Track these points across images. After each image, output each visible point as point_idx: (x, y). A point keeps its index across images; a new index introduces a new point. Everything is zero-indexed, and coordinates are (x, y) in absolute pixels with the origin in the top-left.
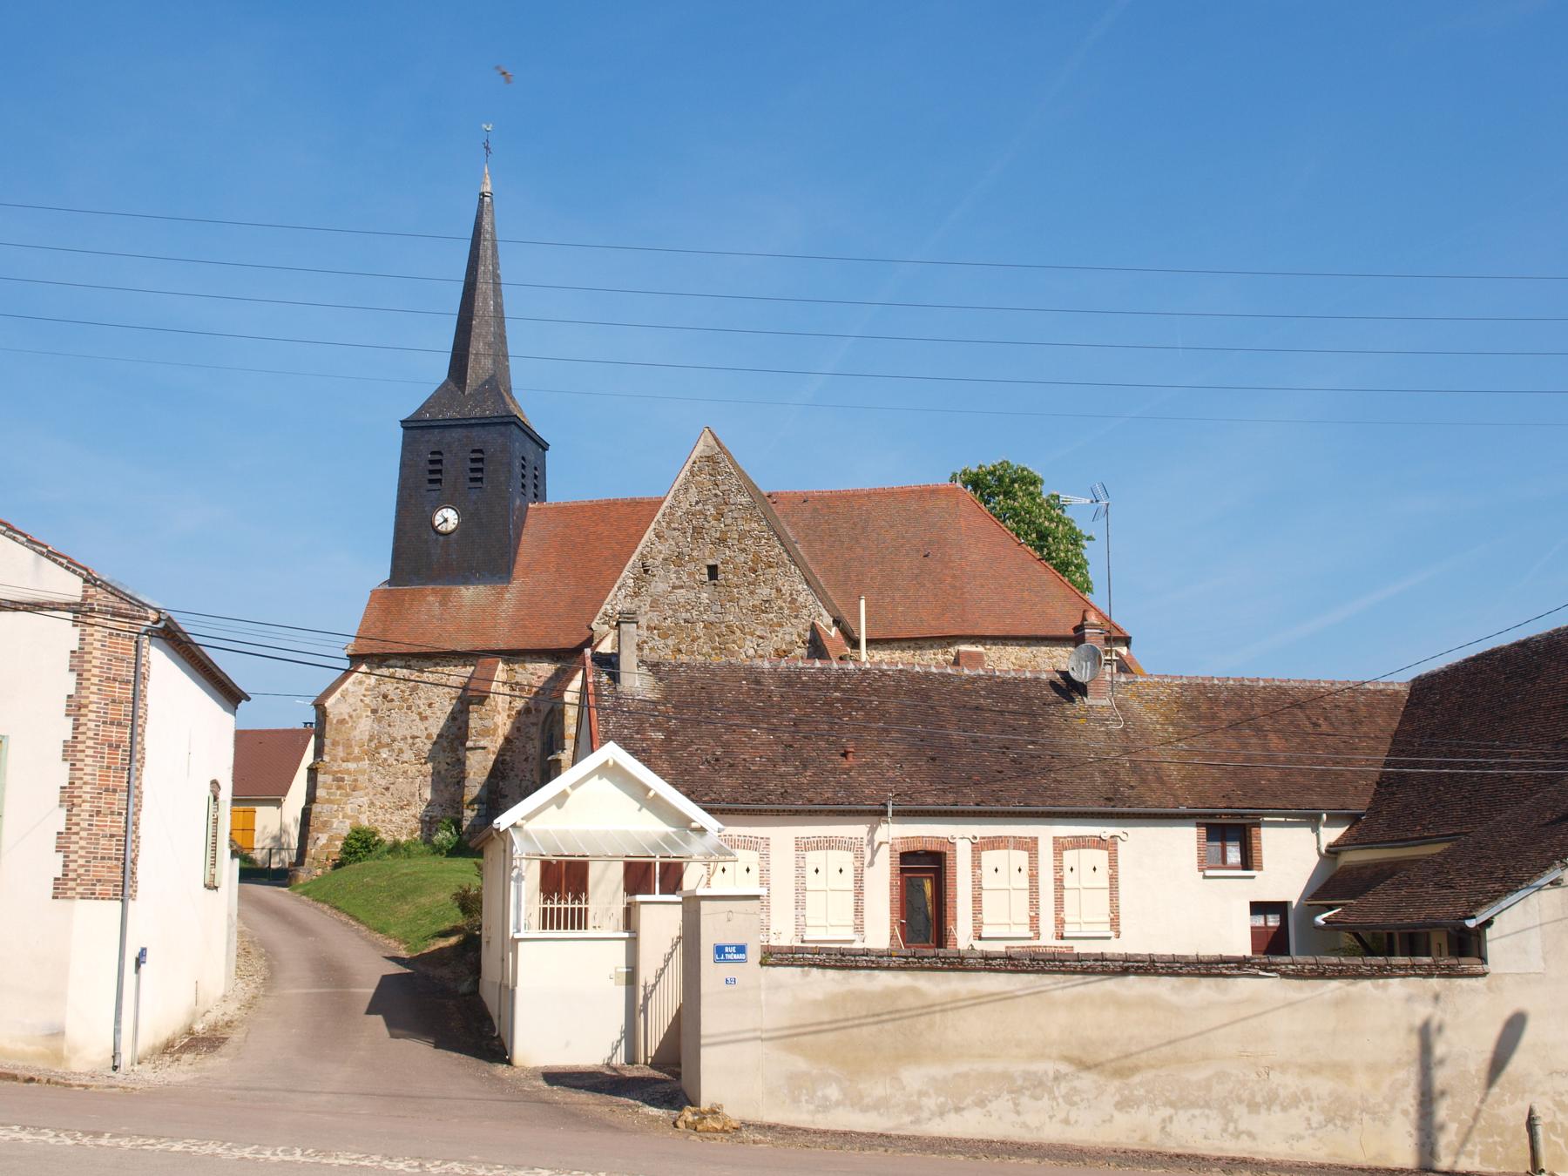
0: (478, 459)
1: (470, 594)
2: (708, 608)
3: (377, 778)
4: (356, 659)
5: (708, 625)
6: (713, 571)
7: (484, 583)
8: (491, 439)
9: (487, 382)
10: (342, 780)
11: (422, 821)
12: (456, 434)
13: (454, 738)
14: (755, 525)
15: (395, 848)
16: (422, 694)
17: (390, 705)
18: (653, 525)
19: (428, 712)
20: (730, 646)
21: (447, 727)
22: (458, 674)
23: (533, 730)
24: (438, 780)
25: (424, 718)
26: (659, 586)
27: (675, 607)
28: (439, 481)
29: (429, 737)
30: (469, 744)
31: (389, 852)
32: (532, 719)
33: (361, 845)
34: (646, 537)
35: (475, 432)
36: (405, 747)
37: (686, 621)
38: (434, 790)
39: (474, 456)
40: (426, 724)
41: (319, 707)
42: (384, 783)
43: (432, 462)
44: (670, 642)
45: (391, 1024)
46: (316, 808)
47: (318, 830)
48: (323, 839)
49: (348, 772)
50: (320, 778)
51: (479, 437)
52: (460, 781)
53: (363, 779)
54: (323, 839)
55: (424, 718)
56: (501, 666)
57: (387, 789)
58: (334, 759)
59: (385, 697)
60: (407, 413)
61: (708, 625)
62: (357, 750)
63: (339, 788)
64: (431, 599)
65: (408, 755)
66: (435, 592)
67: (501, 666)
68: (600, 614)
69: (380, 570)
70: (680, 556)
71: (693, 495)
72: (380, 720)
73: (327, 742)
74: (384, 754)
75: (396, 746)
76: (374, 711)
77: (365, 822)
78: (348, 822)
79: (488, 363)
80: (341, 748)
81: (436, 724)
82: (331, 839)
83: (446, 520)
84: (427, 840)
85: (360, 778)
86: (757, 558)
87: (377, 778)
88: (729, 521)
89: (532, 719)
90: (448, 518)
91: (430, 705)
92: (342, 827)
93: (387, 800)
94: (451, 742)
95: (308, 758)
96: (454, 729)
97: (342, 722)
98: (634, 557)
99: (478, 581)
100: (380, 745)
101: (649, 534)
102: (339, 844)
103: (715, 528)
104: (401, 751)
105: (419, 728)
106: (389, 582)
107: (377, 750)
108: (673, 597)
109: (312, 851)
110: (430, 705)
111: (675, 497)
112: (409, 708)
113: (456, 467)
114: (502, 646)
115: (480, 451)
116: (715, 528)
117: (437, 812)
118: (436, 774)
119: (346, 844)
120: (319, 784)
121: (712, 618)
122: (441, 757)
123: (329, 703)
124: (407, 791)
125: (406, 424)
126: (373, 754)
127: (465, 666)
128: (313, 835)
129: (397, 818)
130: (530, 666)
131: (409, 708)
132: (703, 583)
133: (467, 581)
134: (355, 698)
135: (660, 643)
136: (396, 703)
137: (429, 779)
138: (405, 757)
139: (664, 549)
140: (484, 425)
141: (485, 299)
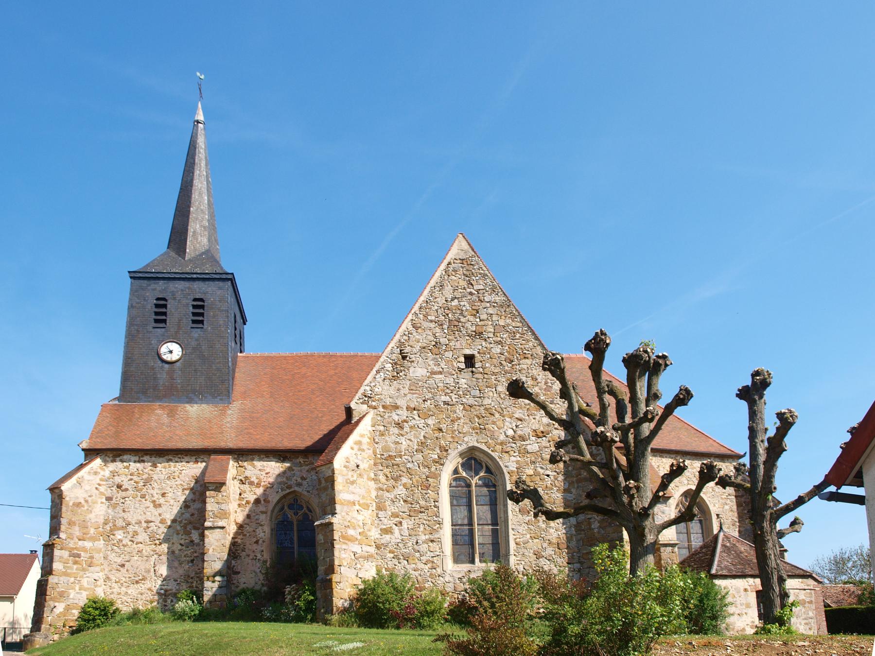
0: (199, 308)
1: (195, 410)
3: (112, 556)
4: (91, 453)
6: (470, 360)
7: (207, 403)
8: (213, 292)
9: (203, 253)
10: (79, 556)
11: (158, 593)
12: (181, 285)
13: (192, 520)
14: (509, 321)
15: (135, 615)
16: (155, 485)
17: (124, 494)
18: (410, 317)
19: (162, 501)
20: (490, 426)
21: (180, 513)
22: (191, 470)
23: (262, 517)
24: (173, 558)
25: (157, 506)
26: (418, 371)
27: (434, 390)
28: (164, 321)
29: (162, 521)
30: (207, 524)
31: (129, 619)
32: (262, 508)
33: (97, 614)
34: (403, 327)
35: (196, 285)
36: (140, 530)
37: (445, 403)
38: (170, 567)
39: (195, 303)
40: (160, 510)
41: (55, 491)
42: (119, 560)
43: (157, 306)
44: (430, 421)
46: (52, 580)
47: (54, 600)
48: (60, 608)
49: (85, 550)
50: (57, 553)
51: (199, 289)
52: (199, 557)
53: (98, 557)
54: (60, 608)
55: (157, 506)
56: (231, 462)
57: (123, 566)
58: (70, 537)
59: (119, 487)
60: (44, 542)
62: (92, 531)
63: (75, 563)
64: (159, 412)
65: (142, 537)
66: (163, 408)
67: (231, 462)
68: (359, 395)
69: (115, 390)
70: (437, 344)
71: (448, 292)
72: (115, 506)
73: (64, 521)
74: (119, 535)
75: (130, 529)
76: (109, 499)
77: (100, 593)
78: (84, 594)
79: (204, 241)
80: (77, 528)
81: (171, 510)
82: (68, 608)
83: (171, 352)
84: (164, 609)
85: (96, 556)
86: (513, 350)
87: (112, 556)
88: (484, 317)
89: (262, 508)
90: (172, 351)
91: (163, 495)
92: (79, 598)
93: (123, 575)
94: (185, 527)
95: (35, 573)
96: (187, 515)
97: (78, 505)
98: (392, 344)
99: (201, 401)
100: (115, 528)
101: (407, 325)
102: (76, 613)
103: (470, 324)
104: (136, 533)
105: (153, 514)
106: (118, 399)
107: (112, 532)
108: (431, 381)
109: (48, 617)
110: (163, 495)
111: (431, 293)
112: (143, 496)
113: (179, 310)
114: (231, 445)
115: (202, 300)
116: (470, 324)
117: (172, 586)
118: (171, 552)
119: (84, 611)
120: (56, 558)
121: (471, 401)
122: (175, 538)
123: (65, 487)
124: (143, 567)
126: (108, 537)
127: (197, 462)
128: (50, 603)
129: (133, 591)
130: (258, 464)
131: (143, 496)
132: (461, 370)
133: (190, 401)
134: (89, 485)
135: (420, 422)
136: (130, 492)
137: (164, 558)
138: (140, 538)
139: (422, 338)
140: (204, 280)
141: (200, 194)
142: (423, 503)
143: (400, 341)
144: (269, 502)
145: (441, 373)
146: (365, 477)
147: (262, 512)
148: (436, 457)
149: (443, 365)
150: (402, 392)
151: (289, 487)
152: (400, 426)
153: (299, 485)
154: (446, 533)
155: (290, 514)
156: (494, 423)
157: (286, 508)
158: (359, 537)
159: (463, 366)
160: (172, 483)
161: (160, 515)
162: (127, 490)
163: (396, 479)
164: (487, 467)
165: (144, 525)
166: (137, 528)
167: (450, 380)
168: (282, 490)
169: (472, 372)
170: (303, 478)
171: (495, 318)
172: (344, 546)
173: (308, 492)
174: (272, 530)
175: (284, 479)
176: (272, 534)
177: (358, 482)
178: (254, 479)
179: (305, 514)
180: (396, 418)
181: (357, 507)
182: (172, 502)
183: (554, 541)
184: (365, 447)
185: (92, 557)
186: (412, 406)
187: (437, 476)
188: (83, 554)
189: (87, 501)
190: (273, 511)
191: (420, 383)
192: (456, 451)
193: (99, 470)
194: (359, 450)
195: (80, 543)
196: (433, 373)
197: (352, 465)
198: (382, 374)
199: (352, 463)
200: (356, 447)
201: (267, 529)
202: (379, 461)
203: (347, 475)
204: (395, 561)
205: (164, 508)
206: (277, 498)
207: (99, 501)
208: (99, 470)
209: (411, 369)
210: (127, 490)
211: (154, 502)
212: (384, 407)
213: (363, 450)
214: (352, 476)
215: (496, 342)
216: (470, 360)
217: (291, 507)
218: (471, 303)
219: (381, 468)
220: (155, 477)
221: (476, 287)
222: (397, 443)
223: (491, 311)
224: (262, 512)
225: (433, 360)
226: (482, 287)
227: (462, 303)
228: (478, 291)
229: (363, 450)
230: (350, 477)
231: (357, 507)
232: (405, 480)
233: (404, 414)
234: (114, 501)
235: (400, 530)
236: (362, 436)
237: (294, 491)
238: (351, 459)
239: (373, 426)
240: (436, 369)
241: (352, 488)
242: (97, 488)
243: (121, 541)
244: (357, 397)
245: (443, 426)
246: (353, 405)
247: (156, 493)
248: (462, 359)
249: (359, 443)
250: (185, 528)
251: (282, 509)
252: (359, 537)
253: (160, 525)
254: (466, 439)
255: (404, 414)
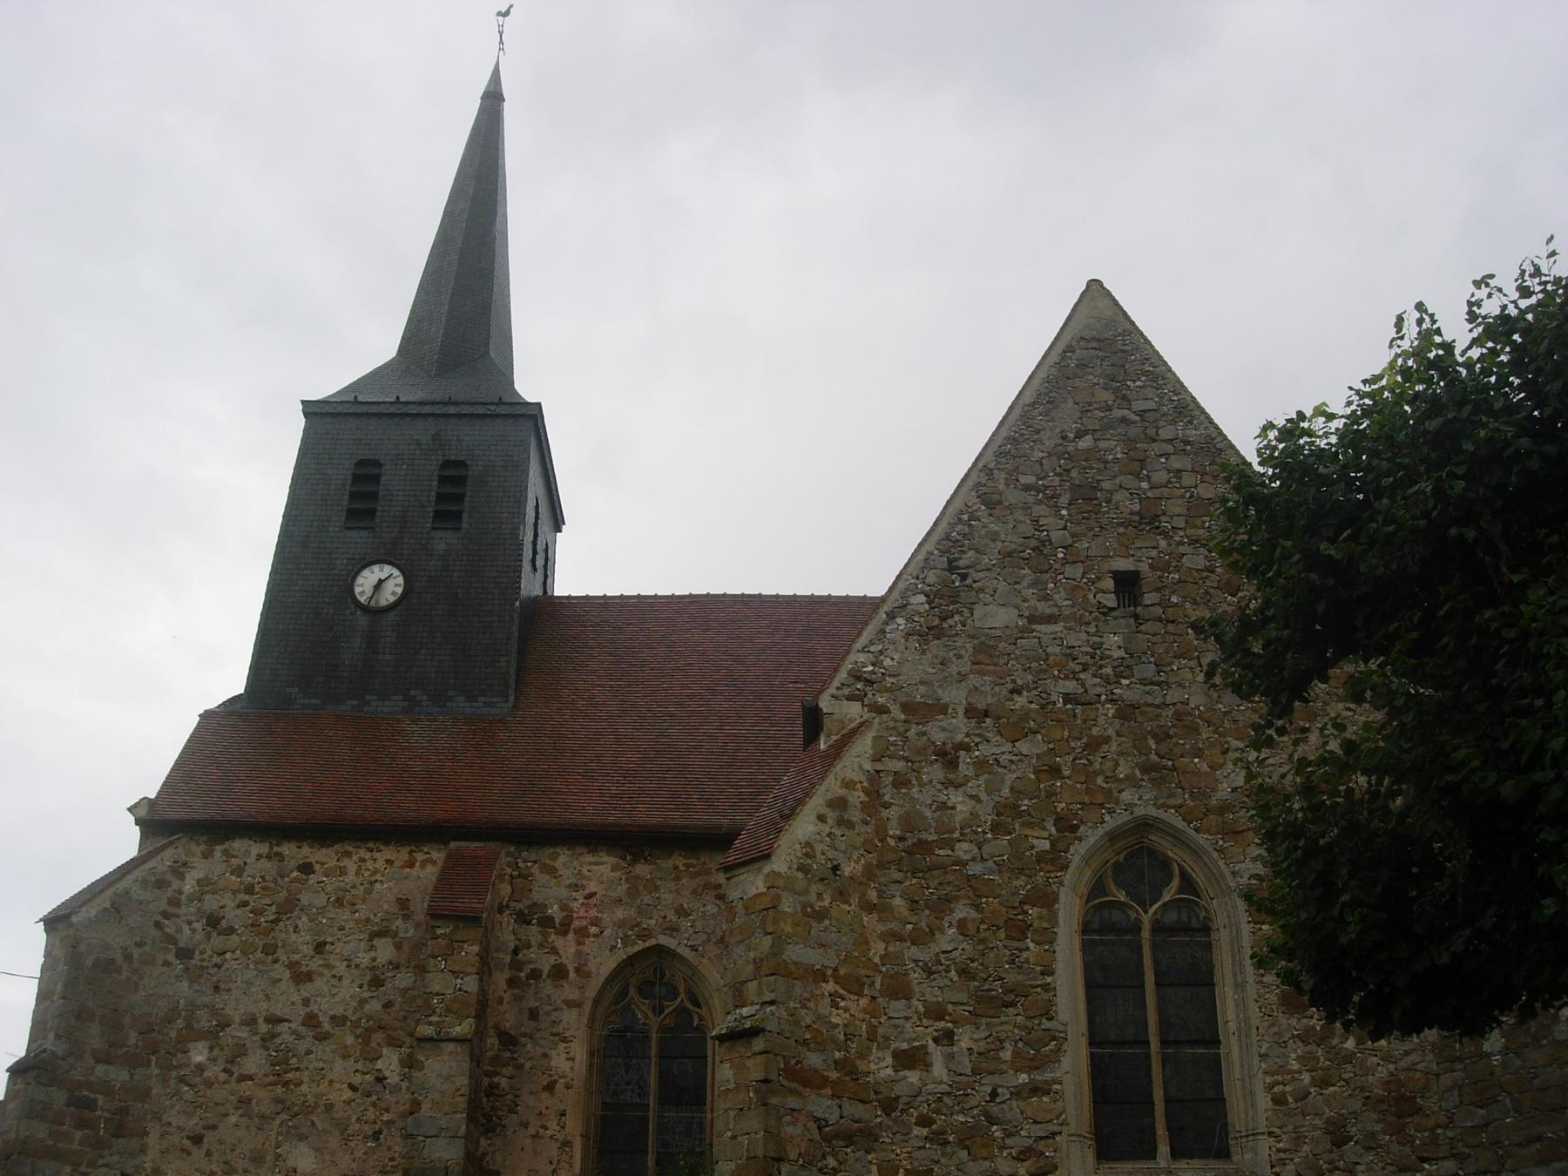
2: (1123, 670)
5: (1127, 712)
6: (1127, 584)
10: (91, 1105)
19: (315, 964)
37: (1068, 698)
42: (193, 1124)
45: (150, 804)
49: (107, 1088)
55: (302, 977)
60: (328, 383)
61: (1127, 712)
62: (133, 1037)
63: (81, 1124)
68: (842, 676)
90: (380, 582)
96: (375, 1006)
104: (241, 1051)
125: (315, 411)
131: (270, 950)
142: (1012, 977)
143: (948, 537)
144: (588, 975)
145: (1051, 619)
146: (855, 899)
147: (570, 1004)
148: (1046, 845)
149: (1061, 598)
150: (954, 669)
151: (645, 934)
152: (948, 757)
153: (672, 930)
154: (1072, 1069)
155: (642, 1011)
156: (1198, 753)
157: (632, 992)
158: (834, 1075)
159: (1111, 601)
160: (344, 915)
161: (306, 1002)
162: (231, 931)
163: (942, 906)
164: (1184, 876)
165: (263, 1028)
166: (244, 1033)
167: (1076, 639)
168: (626, 941)
169: (1136, 617)
170: (682, 912)
171: (1188, 480)
172: (792, 1102)
173: (694, 949)
174: (591, 1053)
175: (632, 912)
176: (590, 1067)
177: (834, 912)
178: (554, 911)
179: (682, 1012)
180: (939, 737)
181: (830, 986)
182: (341, 968)
183: (1329, 1146)
184: (855, 815)
185: (123, 1111)
186: (981, 706)
187: (1047, 900)
188: (101, 1100)
189: (128, 957)
190: (597, 1001)
191: (1002, 645)
192: (1100, 831)
193: (169, 877)
194: (841, 822)
195: (100, 1070)
196: (1033, 619)
197: (819, 864)
198: (900, 620)
199: (820, 858)
200: (831, 816)
201: (579, 1051)
202: (891, 856)
203: (806, 891)
204: (934, 1151)
205: (319, 984)
206: (611, 964)
207: (160, 958)
208: (169, 877)
209: (979, 610)
210: (231, 931)
211: (292, 965)
212: (905, 707)
213: (849, 825)
214: (820, 895)
215: (1194, 542)
216: (1127, 584)
217: (645, 989)
218: (1130, 444)
219: (897, 876)
220: (305, 899)
221: (1139, 405)
222: (943, 806)
223: (1176, 463)
224: (570, 1004)
225: (1032, 585)
226: (1151, 405)
227: (1102, 444)
228: (1142, 413)
229: (849, 825)
230: (813, 898)
231: (830, 986)
232: (962, 911)
233: (959, 727)
234: (195, 961)
235: (950, 1057)
236: (849, 784)
237: (659, 949)
238: (819, 848)
239: (877, 759)
240: (1044, 608)
241: (816, 928)
242: (158, 925)
243: (200, 1068)
244: (836, 683)
245: (1065, 762)
246: (825, 703)
247: (299, 940)
248: (1109, 584)
249: (839, 804)
250: (367, 1042)
251: (624, 993)
252: (834, 1075)
253: (302, 1030)
254: (1126, 796)
255: (959, 727)
